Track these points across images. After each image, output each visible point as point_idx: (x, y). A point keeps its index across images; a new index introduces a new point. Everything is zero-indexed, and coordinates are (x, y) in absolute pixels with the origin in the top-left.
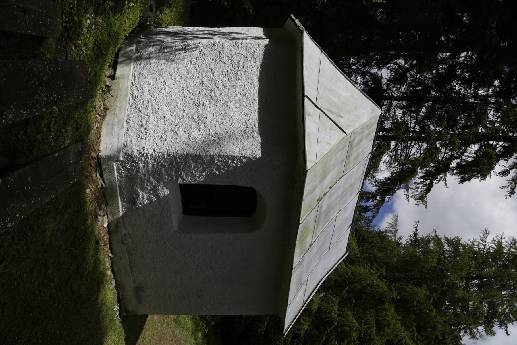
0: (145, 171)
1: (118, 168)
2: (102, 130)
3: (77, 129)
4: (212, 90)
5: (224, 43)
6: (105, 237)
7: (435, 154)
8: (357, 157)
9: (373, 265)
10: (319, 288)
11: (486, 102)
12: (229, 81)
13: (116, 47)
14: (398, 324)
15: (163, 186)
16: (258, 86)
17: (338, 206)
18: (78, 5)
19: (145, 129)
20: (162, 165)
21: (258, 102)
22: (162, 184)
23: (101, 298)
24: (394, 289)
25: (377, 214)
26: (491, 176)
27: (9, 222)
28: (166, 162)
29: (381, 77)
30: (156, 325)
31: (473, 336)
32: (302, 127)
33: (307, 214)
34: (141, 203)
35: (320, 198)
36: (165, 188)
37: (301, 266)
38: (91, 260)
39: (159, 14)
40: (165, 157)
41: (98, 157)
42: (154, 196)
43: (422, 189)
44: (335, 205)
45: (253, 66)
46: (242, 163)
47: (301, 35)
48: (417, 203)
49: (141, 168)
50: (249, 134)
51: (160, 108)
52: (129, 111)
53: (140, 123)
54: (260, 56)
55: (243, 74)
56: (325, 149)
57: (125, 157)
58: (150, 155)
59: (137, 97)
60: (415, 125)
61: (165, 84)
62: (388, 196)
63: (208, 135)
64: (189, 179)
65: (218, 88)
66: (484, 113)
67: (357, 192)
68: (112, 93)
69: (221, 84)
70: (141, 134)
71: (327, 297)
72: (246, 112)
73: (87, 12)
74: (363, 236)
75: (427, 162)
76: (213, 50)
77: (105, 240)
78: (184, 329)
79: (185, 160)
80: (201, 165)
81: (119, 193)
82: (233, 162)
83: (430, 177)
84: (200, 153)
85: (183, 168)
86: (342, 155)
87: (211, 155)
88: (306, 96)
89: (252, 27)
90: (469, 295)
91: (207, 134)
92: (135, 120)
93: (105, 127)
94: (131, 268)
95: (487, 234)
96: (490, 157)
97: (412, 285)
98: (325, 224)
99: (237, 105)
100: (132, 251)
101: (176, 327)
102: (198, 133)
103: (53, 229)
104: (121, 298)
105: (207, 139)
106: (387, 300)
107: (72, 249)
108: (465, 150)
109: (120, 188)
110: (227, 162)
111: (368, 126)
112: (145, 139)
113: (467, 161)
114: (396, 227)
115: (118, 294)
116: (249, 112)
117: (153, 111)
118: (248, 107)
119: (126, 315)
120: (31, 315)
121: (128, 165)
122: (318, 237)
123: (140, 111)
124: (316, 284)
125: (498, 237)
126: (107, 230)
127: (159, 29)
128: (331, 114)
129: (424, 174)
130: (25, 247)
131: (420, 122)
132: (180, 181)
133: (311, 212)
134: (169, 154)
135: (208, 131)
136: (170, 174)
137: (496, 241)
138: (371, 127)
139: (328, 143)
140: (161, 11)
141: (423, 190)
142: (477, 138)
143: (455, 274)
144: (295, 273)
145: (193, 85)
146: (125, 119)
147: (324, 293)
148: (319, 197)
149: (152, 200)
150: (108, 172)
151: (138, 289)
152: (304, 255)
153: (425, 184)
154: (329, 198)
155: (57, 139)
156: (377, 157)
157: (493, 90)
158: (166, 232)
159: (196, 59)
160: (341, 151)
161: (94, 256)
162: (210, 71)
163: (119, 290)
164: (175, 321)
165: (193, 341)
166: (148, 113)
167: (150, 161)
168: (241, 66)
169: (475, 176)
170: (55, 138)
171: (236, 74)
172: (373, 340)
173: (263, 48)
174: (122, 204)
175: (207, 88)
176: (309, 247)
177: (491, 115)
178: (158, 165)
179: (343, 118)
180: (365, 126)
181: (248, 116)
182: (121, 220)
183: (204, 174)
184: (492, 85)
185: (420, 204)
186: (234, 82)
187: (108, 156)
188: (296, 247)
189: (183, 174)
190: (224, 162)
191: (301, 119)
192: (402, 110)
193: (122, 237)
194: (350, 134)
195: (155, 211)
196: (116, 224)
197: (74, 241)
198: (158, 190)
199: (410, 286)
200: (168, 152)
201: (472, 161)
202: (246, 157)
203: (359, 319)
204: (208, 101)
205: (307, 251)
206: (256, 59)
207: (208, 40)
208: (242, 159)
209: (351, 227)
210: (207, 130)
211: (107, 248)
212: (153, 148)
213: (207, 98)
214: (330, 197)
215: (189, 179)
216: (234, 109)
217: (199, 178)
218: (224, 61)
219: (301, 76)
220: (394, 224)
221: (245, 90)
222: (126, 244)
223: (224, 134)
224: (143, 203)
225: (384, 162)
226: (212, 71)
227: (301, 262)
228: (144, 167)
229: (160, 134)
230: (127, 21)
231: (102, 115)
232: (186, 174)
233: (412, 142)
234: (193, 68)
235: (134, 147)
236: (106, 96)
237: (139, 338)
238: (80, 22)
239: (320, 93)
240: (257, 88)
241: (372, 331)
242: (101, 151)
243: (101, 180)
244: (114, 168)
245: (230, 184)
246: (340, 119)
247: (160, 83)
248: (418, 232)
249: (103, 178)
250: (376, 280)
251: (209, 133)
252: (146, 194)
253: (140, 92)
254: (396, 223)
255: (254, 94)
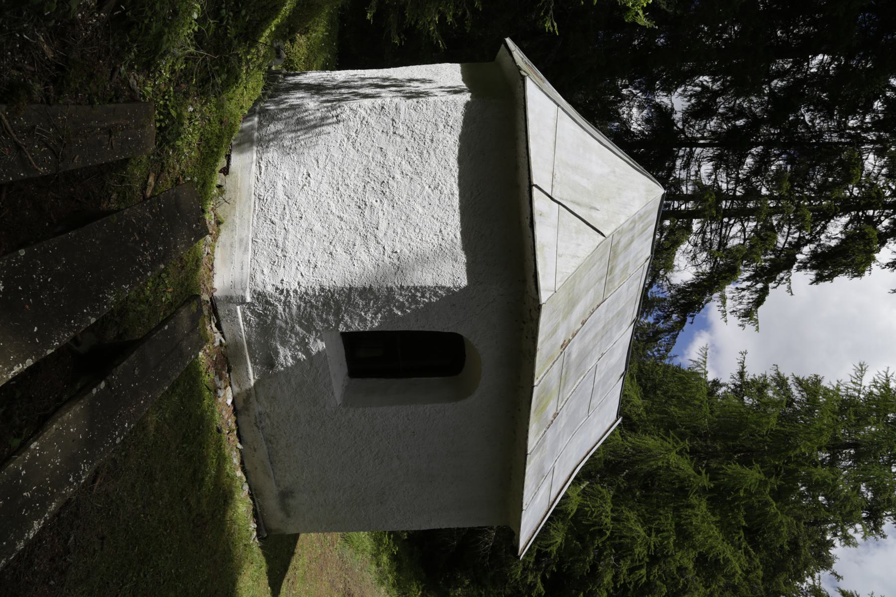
0: (286, 317)
1: (243, 313)
2: (215, 256)
4: (383, 182)
5: (398, 103)
6: (230, 420)
7: (769, 238)
8: (626, 267)
9: (667, 434)
11: (857, 141)
14: (712, 529)
15: (316, 338)
16: (458, 171)
18: (175, 92)
19: (282, 250)
20: (312, 306)
21: (458, 198)
22: (314, 334)
25: (673, 345)
26: (870, 270)
28: (318, 301)
29: (672, 109)
30: (313, 546)
32: (531, 236)
33: (546, 370)
35: (567, 341)
36: (319, 341)
37: (542, 448)
38: (213, 458)
39: (289, 46)
40: (317, 294)
42: (303, 353)
43: (749, 299)
44: (593, 348)
46: (438, 297)
47: (522, 85)
48: (741, 323)
49: (279, 312)
50: (446, 251)
51: (304, 216)
52: (255, 223)
53: (273, 241)
54: (458, 122)
55: (432, 153)
56: (568, 267)
57: (253, 297)
58: (293, 292)
59: (267, 199)
60: (736, 187)
61: (309, 176)
62: (691, 314)
63: (381, 256)
64: (356, 325)
65: (393, 178)
66: (855, 164)
68: (227, 196)
70: (277, 259)
71: (592, 488)
72: (441, 215)
73: (187, 96)
74: (653, 379)
75: (756, 253)
76: (382, 117)
77: (230, 424)
78: (358, 550)
79: (349, 296)
80: (374, 303)
81: (248, 351)
82: (423, 296)
83: (763, 277)
84: (371, 285)
85: (345, 308)
86: (600, 269)
87: (389, 286)
88: (534, 185)
89: (443, 64)
90: (832, 476)
92: (266, 237)
93: (219, 251)
94: (271, 463)
95: (863, 372)
96: (867, 241)
97: (735, 464)
98: (578, 379)
99: (426, 203)
100: (272, 438)
101: (345, 547)
102: (366, 253)
104: (258, 509)
105: (380, 262)
106: (692, 491)
107: (184, 446)
109: (249, 343)
110: (414, 296)
112: (284, 267)
114: (705, 367)
115: (254, 505)
116: (444, 215)
117: (292, 221)
118: (444, 206)
119: (268, 535)
120: (136, 550)
121: (259, 309)
122: (566, 401)
123: (272, 223)
124: (589, 448)
125: (880, 376)
126: (232, 408)
128: (578, 207)
129: (753, 273)
130: (123, 454)
132: (342, 328)
133: (552, 366)
134: (322, 289)
135: (381, 249)
136: (326, 319)
137: (877, 382)
138: (648, 217)
139: (574, 256)
140: (292, 41)
141: (751, 301)
142: (846, 206)
143: (809, 441)
144: (532, 462)
146: (250, 236)
147: (588, 483)
148: (565, 341)
149: (300, 360)
150: (229, 321)
151: (285, 495)
152: (545, 431)
153: (754, 290)
154: (581, 339)
155: (155, 290)
157: (872, 118)
159: (356, 133)
160: (598, 264)
161: (216, 452)
162: (379, 150)
163: (255, 497)
164: (344, 538)
166: (286, 225)
167: (293, 300)
168: (428, 140)
169: (841, 272)
170: (153, 288)
171: (421, 154)
173: (461, 108)
174: (253, 368)
175: (376, 180)
176: (553, 419)
177: (871, 162)
179: (598, 210)
180: (637, 218)
181: (444, 221)
182: (253, 392)
183: (379, 316)
184: (868, 109)
185: (747, 325)
186: (418, 166)
188: (530, 421)
189: (346, 318)
190: (410, 297)
191: (528, 221)
192: (711, 163)
193: (256, 417)
194: (611, 236)
195: (305, 376)
196: (245, 398)
197: (187, 435)
198: (307, 344)
199: (731, 464)
200: (320, 286)
201: (836, 247)
202: (444, 287)
203: (645, 521)
204: (379, 200)
205: (550, 425)
206: (451, 127)
207: (373, 100)
208: (437, 290)
209: (622, 377)
210: (380, 248)
211: (233, 437)
212: (297, 280)
213: (376, 196)
215: (356, 325)
216: (421, 211)
217: (372, 322)
218: (401, 134)
219: (526, 153)
220: (702, 362)
221: (436, 179)
222: (262, 428)
223: (408, 252)
224: (286, 365)
225: (684, 252)
226: (382, 151)
227: (540, 444)
228: (284, 310)
229: (306, 258)
230: (245, 92)
231: (214, 232)
232: (351, 318)
233: (730, 220)
234: (352, 148)
235: (267, 280)
236: (217, 202)
237: (288, 569)
238: (180, 116)
239: (558, 175)
240: (456, 175)
242: (215, 290)
243: (219, 334)
244: (237, 315)
245: (421, 329)
246: (594, 213)
247: (301, 175)
248: (745, 370)
249: (221, 330)
250: (673, 458)
251: (384, 252)
252: (290, 350)
253: (270, 191)
254: (704, 359)
255: (452, 185)
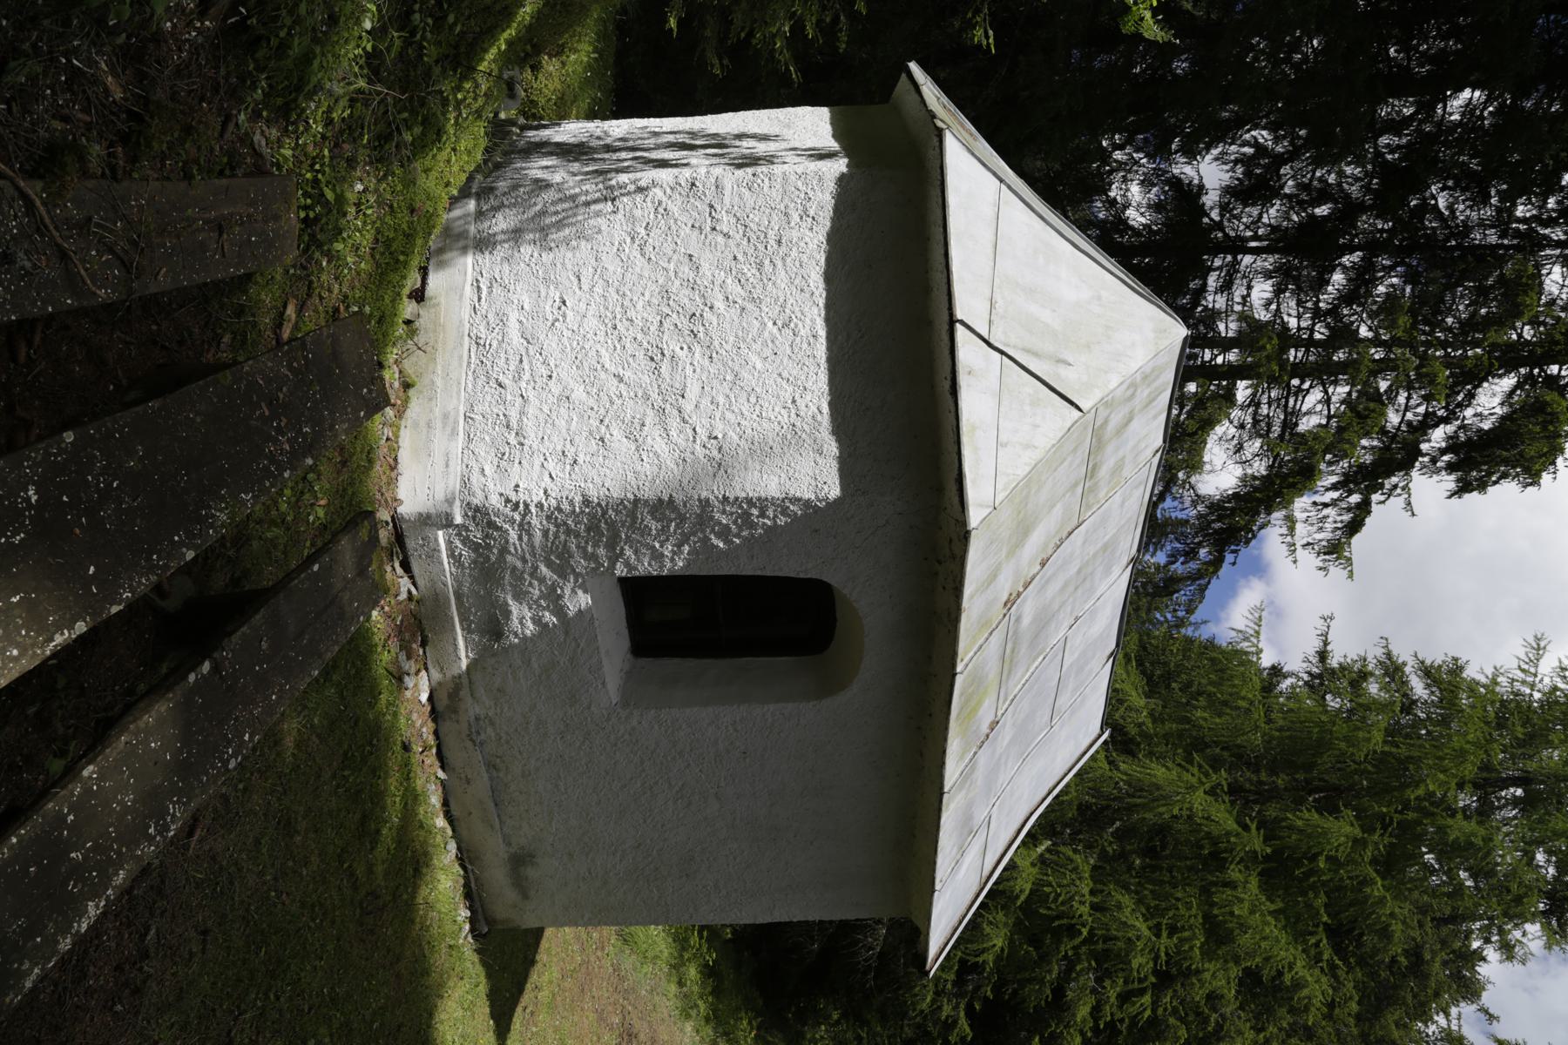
1: (449, 543)
3: (344, 463)
4: (694, 314)
6: (424, 730)
8: (1119, 467)
10: (1033, 827)
12: (742, 286)
13: (430, 234)
14: (1268, 924)
16: (824, 295)
17: (1069, 609)
18: (332, 158)
20: (568, 532)
23: (424, 891)
24: (1253, 827)
25: (1201, 602)
27: (232, 756)
28: (579, 523)
31: (1508, 950)
32: (953, 409)
34: (516, 635)
36: (580, 592)
40: (577, 510)
41: (396, 519)
42: (552, 613)
45: (807, 239)
46: (789, 516)
48: (1321, 564)
49: (511, 541)
50: (804, 436)
51: (554, 375)
53: (502, 417)
54: (825, 209)
55: (779, 263)
56: (1018, 465)
57: (466, 515)
62: (1233, 547)
63: (690, 444)
65: (711, 308)
67: (1125, 560)
68: (421, 339)
69: (721, 297)
76: (692, 200)
77: (425, 736)
79: (632, 514)
80: (677, 526)
82: (762, 515)
86: (1073, 468)
88: (958, 321)
91: (687, 440)
97: (1309, 810)
103: (299, 730)
104: (473, 885)
107: (346, 773)
108: (1471, 396)
109: (458, 596)
110: (747, 514)
111: (1147, 378)
113: (1481, 430)
115: (466, 878)
121: (477, 535)
123: (500, 385)
124: (1051, 784)
127: (535, 133)
130: (241, 786)
131: (1328, 312)
132: (620, 570)
134: (586, 502)
135: (690, 432)
138: (1158, 377)
139: (1027, 446)
140: (536, 68)
141: (1339, 525)
142: (1509, 358)
144: (952, 806)
145: (641, 304)
146: (462, 409)
149: (546, 625)
151: (519, 861)
152: (975, 753)
155: (297, 501)
156: (1195, 433)
158: (589, 708)
159: (646, 228)
160: (1069, 459)
162: (687, 259)
165: (673, 988)
167: (535, 521)
168: (772, 242)
170: (293, 499)
171: (760, 266)
172: (1198, 972)
173: (831, 186)
178: (558, 531)
180: (1139, 379)
181: (799, 383)
182: (465, 681)
183: (686, 548)
185: (1332, 568)
187: (420, 514)
189: (628, 552)
190: (739, 516)
191: (947, 384)
192: (1270, 282)
198: (560, 597)
202: (799, 500)
204: (685, 347)
207: (675, 171)
211: (431, 759)
212: (543, 485)
214: (1043, 588)
216: (759, 365)
217: (672, 560)
218: (725, 231)
222: (481, 744)
223: (736, 438)
225: (1220, 439)
227: (966, 775)
228: (520, 538)
229: (559, 448)
230: (454, 158)
231: (399, 402)
232: (636, 552)
233: (1303, 382)
235: (491, 486)
238: (340, 199)
239: (1000, 304)
240: (821, 302)
241: (1191, 948)
242: (401, 502)
245: (759, 573)
246: (1063, 371)
247: (550, 302)
248: (1329, 648)
250: (1199, 800)
253: (496, 330)
